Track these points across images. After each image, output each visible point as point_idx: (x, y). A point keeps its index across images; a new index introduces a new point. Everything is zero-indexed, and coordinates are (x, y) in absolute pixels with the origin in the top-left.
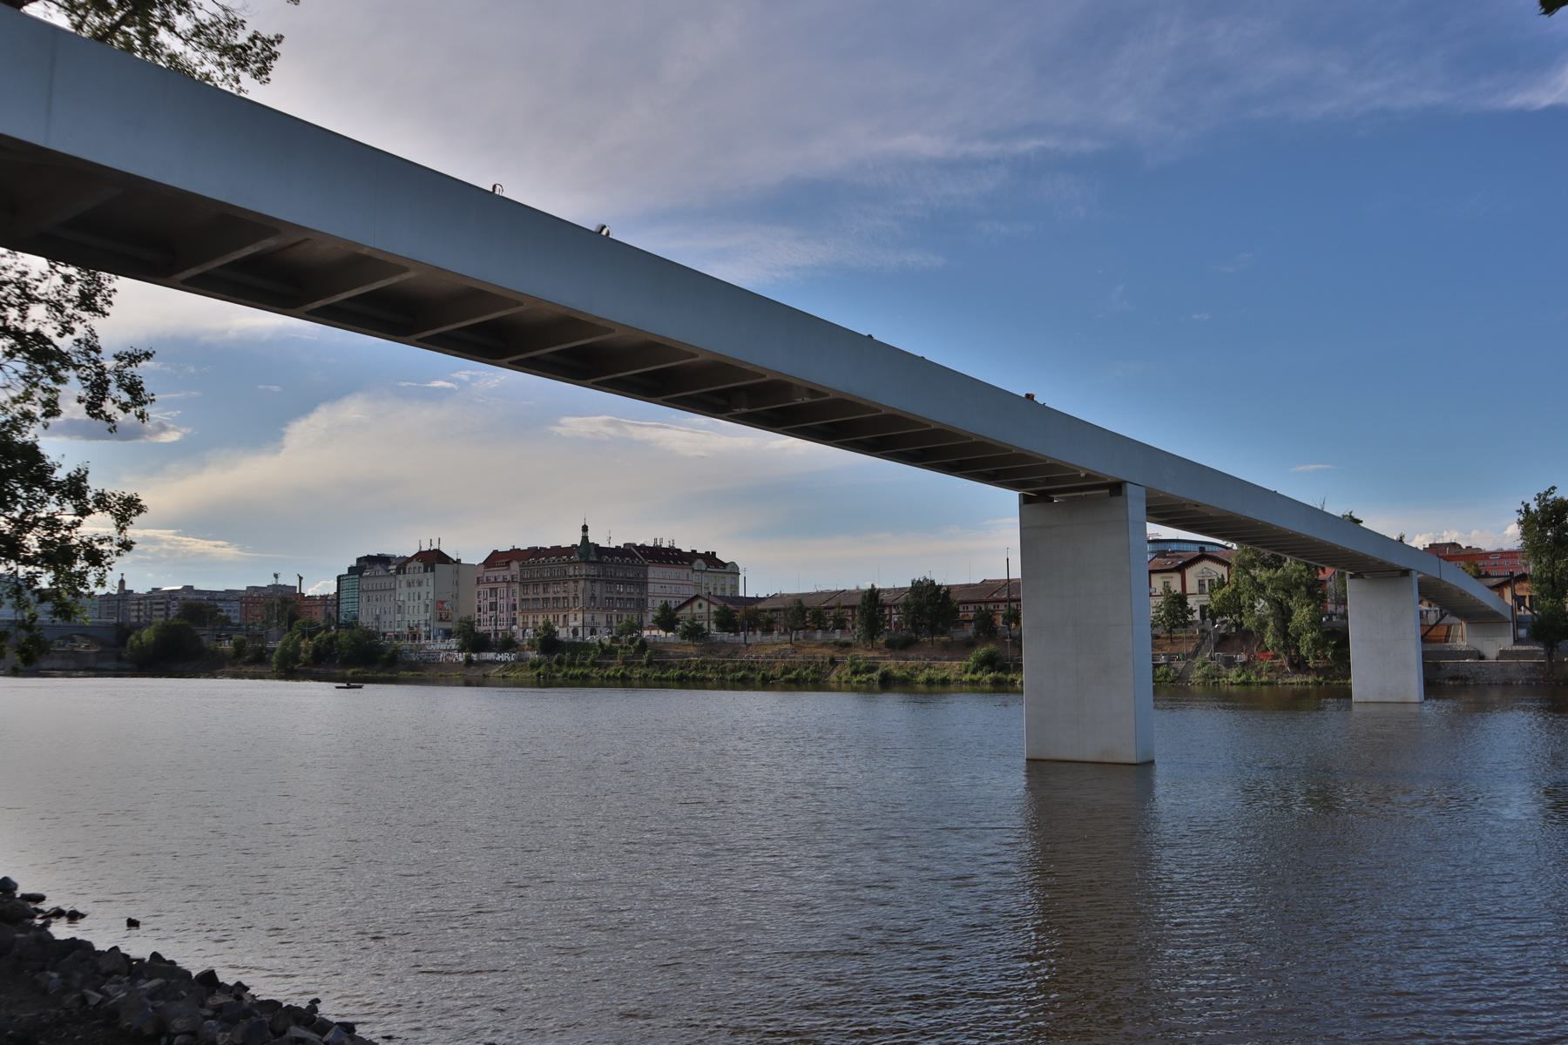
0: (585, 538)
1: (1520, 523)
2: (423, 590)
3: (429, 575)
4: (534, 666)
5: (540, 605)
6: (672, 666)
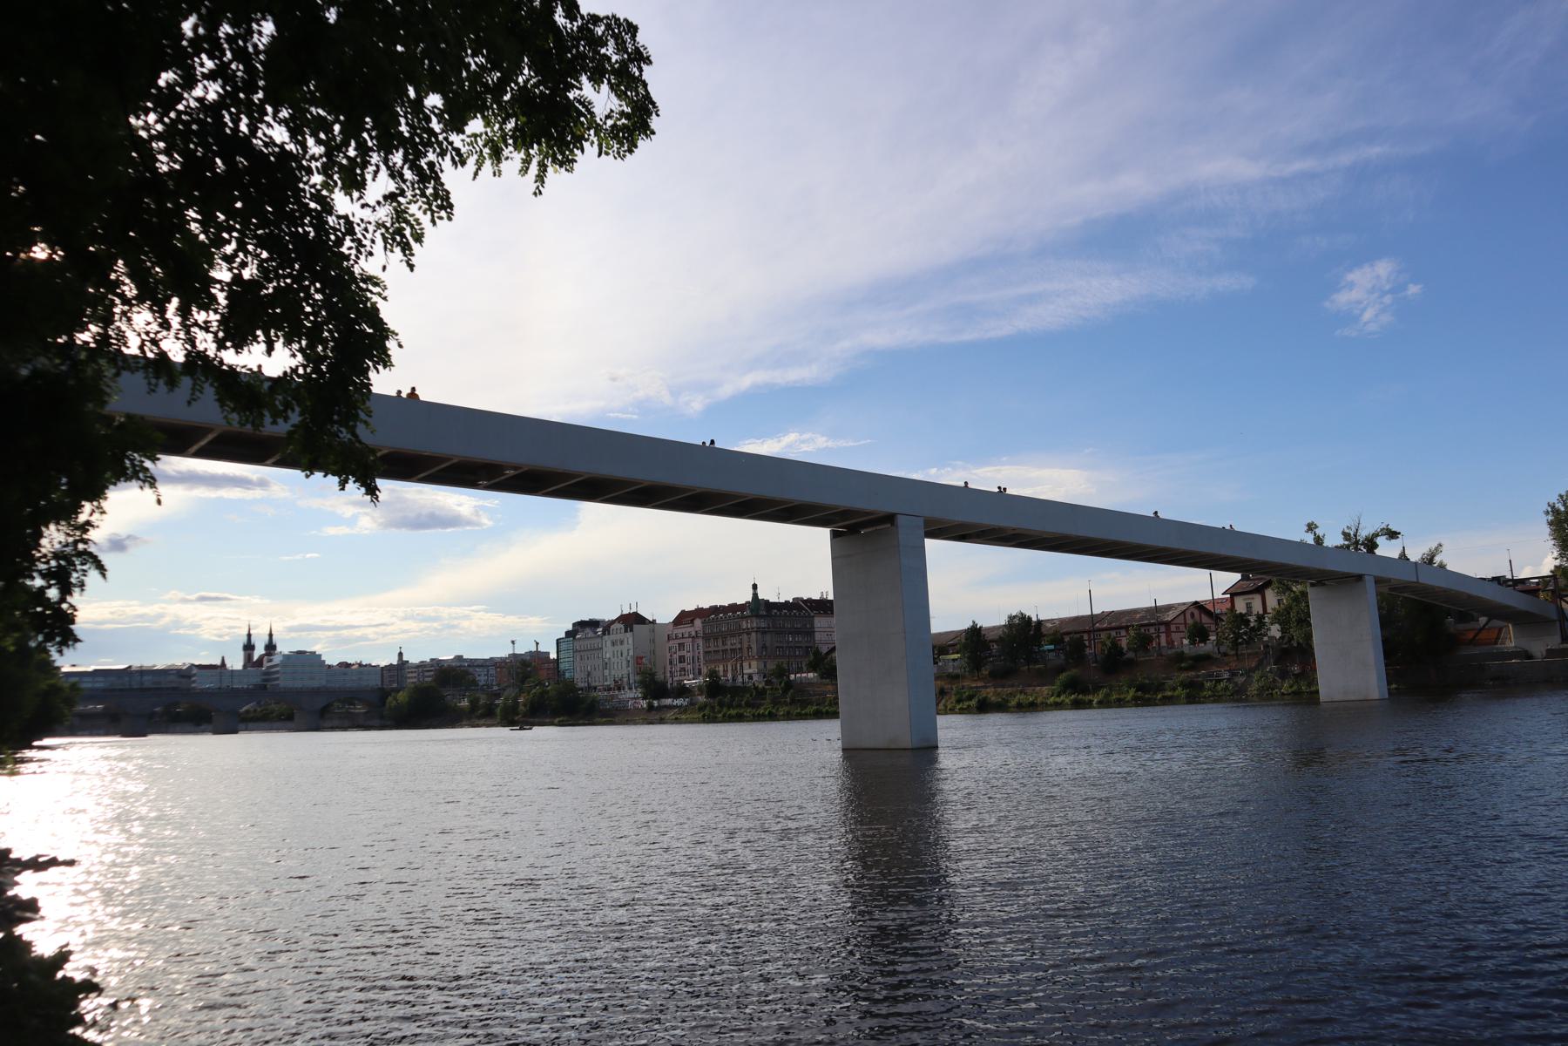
0: (755, 595)
1: (1551, 523)
2: (624, 648)
3: (629, 634)
4: (702, 708)
5: (719, 656)
6: (811, 703)
